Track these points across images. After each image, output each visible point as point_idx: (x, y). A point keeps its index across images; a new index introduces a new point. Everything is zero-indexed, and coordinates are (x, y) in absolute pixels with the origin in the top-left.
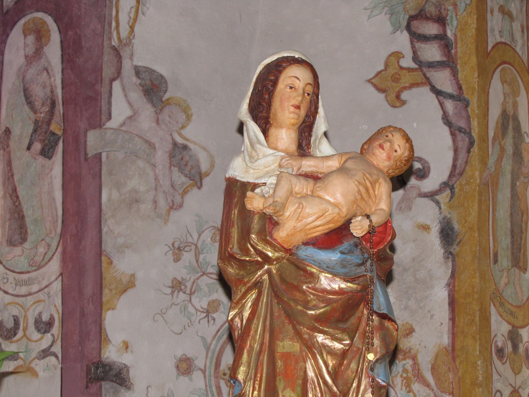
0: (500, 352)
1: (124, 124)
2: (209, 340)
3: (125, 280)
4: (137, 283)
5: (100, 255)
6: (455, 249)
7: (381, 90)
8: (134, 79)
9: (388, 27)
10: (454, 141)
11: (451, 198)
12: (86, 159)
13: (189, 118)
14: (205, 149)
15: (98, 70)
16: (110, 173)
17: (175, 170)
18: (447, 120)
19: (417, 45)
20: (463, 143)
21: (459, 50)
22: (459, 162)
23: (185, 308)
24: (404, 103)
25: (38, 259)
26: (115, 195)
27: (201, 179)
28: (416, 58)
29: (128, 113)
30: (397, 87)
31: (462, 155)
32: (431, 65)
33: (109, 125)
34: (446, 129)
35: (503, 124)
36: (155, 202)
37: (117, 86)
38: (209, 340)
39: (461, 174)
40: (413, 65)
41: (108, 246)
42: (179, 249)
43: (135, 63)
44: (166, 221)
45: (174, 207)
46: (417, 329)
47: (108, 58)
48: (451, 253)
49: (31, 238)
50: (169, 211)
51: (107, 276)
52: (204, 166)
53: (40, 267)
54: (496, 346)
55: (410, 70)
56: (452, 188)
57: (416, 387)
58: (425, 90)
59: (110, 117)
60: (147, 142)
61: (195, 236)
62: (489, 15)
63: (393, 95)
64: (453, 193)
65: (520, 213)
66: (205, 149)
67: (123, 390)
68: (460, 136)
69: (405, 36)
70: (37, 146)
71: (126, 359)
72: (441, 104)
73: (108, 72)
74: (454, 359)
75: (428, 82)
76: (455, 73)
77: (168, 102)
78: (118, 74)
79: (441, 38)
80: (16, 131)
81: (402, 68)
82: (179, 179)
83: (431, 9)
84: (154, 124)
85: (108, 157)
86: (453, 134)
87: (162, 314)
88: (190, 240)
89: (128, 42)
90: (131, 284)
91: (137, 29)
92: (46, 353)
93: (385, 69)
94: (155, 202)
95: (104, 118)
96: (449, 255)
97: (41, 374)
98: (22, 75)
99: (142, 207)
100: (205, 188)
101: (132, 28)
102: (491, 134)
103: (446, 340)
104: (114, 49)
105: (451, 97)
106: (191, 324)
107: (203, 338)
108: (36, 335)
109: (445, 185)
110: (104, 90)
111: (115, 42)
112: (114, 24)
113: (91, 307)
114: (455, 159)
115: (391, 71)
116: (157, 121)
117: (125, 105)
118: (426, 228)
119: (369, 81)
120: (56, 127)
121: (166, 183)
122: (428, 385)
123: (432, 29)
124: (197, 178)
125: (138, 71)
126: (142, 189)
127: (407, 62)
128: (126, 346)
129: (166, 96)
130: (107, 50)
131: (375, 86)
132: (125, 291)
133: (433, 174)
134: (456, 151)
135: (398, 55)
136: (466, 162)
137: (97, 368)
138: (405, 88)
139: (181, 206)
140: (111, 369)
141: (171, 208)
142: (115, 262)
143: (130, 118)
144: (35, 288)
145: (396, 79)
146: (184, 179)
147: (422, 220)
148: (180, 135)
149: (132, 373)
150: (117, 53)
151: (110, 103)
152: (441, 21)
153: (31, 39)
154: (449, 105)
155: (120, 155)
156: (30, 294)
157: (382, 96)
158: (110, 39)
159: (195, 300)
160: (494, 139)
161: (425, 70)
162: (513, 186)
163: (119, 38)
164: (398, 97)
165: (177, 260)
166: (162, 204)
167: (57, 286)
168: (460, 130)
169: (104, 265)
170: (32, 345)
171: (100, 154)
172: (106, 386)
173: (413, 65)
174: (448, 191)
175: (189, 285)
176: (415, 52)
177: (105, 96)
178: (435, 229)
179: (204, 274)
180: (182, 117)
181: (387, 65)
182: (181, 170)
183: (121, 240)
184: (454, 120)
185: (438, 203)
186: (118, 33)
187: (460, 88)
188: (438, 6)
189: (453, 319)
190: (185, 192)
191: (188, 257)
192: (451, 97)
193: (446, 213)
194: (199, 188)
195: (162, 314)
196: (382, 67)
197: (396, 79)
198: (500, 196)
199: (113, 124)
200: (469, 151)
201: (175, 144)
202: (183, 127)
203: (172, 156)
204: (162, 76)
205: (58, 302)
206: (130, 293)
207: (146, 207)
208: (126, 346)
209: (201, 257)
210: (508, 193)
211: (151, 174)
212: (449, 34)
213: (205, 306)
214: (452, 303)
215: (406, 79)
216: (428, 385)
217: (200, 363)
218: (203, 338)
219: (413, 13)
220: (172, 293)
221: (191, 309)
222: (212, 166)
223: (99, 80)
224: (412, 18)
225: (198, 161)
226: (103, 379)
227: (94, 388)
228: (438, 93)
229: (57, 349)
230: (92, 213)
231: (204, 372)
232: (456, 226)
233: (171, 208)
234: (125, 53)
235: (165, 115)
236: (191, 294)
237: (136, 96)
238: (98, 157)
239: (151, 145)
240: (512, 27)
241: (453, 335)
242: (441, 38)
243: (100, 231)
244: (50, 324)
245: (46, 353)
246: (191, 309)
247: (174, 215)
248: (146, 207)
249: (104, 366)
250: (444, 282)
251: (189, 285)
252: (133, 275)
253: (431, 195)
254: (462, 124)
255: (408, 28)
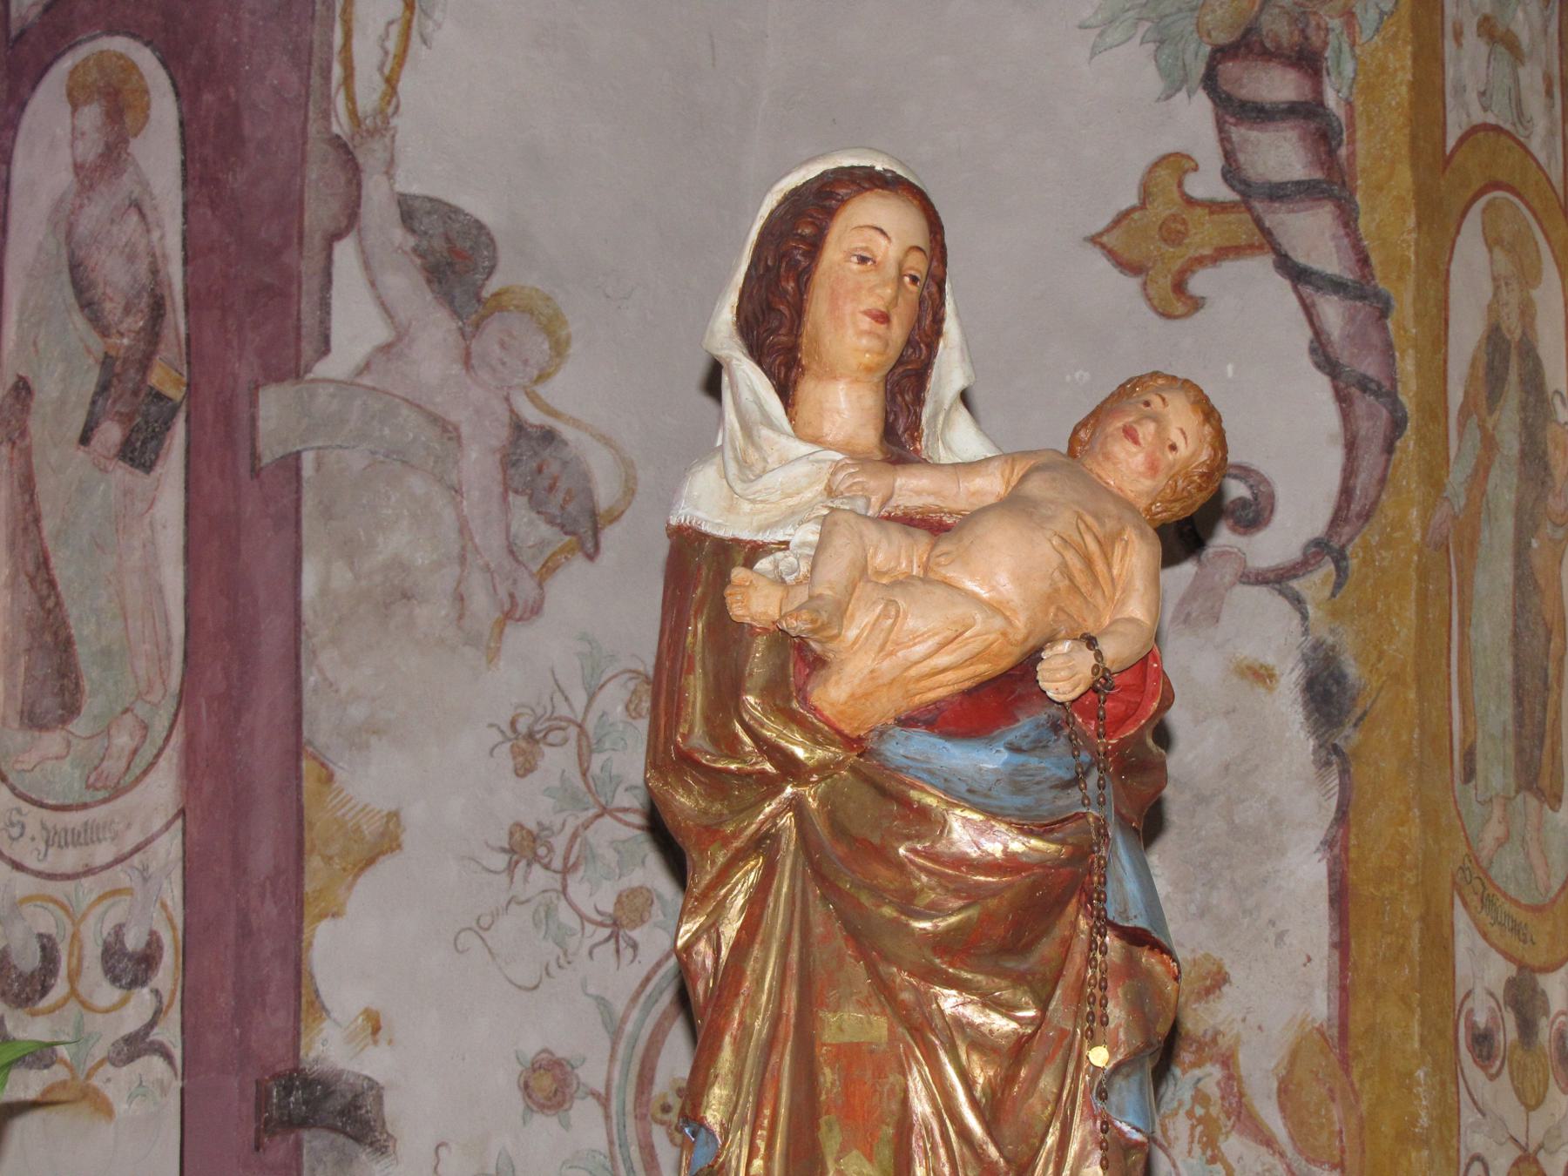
0: (1483, 1042)
1: (366, 367)
2: (619, 1007)
3: (370, 829)
4: (406, 839)
5: (298, 755)
6: (1349, 737)
7: (1130, 267)
8: (398, 234)
9: (1151, 80)
10: (1346, 416)
11: (1338, 586)
12: (255, 472)
13: (559, 348)
14: (607, 441)
15: (290, 207)
16: (327, 513)
17: (519, 502)
18: (1323, 356)
19: (1237, 133)
20: (1372, 425)
21: (1361, 148)
22: (1362, 481)
23: (550, 911)
24: (1196, 304)
25: (114, 766)
26: (342, 577)
27: (596, 532)
28: (1232, 173)
29: (380, 333)
30: (1176, 257)
31: (1370, 459)
32: (1279, 193)
33: (322, 369)
34: (1322, 382)
35: (1490, 368)
36: (460, 598)
37: (345, 254)
38: (619, 1007)
39: (1366, 516)
40: (1225, 194)
41: (320, 727)
42: (530, 736)
43: (400, 187)
44: (493, 655)
45: (515, 612)
46: (1236, 973)
47: (319, 171)
48: (1336, 749)
49: (92, 705)
50: (500, 626)
51: (318, 818)
52: (605, 493)
53: (117, 792)
54: (1472, 1026)
55: (1214, 207)
56: (1340, 558)
57: (1234, 1145)
58: (1261, 267)
59: (325, 348)
60: (437, 421)
61: (579, 698)
62: (1449, 44)
63: (1166, 282)
64: (1342, 572)
65: (1541, 631)
66: (607, 441)
67: (363, 1154)
68: (1363, 404)
69: (1202, 106)
70: (111, 434)
71: (373, 1064)
72: (1308, 310)
73: (319, 212)
74: (1345, 1063)
75: (1268, 242)
76: (1347, 218)
77: (498, 303)
78: (350, 218)
79: (1308, 112)
80: (47, 389)
81: (1190, 202)
82: (532, 529)
83: (1278, 28)
84: (457, 369)
85: (319, 465)
86: (1342, 398)
87: (480, 929)
88: (563, 710)
89: (381, 125)
90: (387, 841)
91: (405, 85)
92: (136, 1046)
93: (1143, 206)
94: (460, 598)
95: (308, 349)
96: (1332, 755)
97: (121, 1107)
98: (65, 224)
99: (422, 612)
100: (607, 556)
101: (391, 82)
102: (1456, 396)
103: (1321, 1007)
104: (338, 144)
105: (1337, 286)
106: (566, 959)
107: (602, 1002)
108: (107, 994)
109: (1319, 548)
110: (309, 267)
111: (340, 125)
112: (337, 71)
113: (271, 909)
114: (1349, 472)
115: (1160, 210)
116: (467, 360)
117: (372, 311)
118: (1261, 675)
119: (1094, 240)
120: (166, 377)
121: (491, 543)
122: (1269, 1142)
123: (1279, 86)
124: (585, 528)
125: (408, 211)
126: (421, 559)
127: (1207, 184)
128: (374, 1025)
129: (493, 285)
130: (317, 148)
131: (1111, 254)
132: (371, 861)
133: (1283, 516)
134: (1351, 446)
135: (1178, 163)
136: (1383, 481)
137: (288, 1090)
138: (1200, 261)
139: (536, 610)
140: (328, 1093)
141: (508, 616)
142: (341, 776)
143: (386, 349)
144: (103, 853)
145: (1173, 233)
146: (545, 530)
147: (1252, 650)
148: (534, 399)
149: (391, 1106)
150: (346, 156)
151: (325, 306)
152: (1308, 61)
153: (92, 115)
154: (1332, 311)
155: (356, 460)
156: (89, 871)
157: (1132, 284)
158: (326, 115)
159: (577, 889)
160: (1465, 412)
161: (1258, 206)
162: (1521, 552)
163: (353, 113)
164: (1179, 287)
165: (524, 769)
166: (481, 603)
167: (169, 847)
168: (1364, 384)
169: (309, 784)
170: (96, 1022)
171: (298, 455)
172: (315, 1142)
173: (1225, 194)
174: (1328, 567)
175: (560, 843)
176: (1229, 155)
177: (310, 285)
178: (1290, 678)
179: (604, 811)
180: (539, 347)
181: (1146, 193)
182: (537, 505)
183: (357, 712)
184: (1344, 356)
185: (1297, 601)
186: (351, 98)
187: (1364, 261)
188: (1299, 18)
189: (1342, 946)
190: (549, 569)
191: (557, 760)
192: (1337, 286)
193: (1322, 631)
194: (591, 557)
195: (480, 929)
196: (1132, 199)
197: (1173, 233)
198: (1481, 581)
199: (335, 366)
200: (1389, 449)
201: (519, 427)
202: (543, 377)
203: (508, 462)
204: (481, 227)
205: (173, 893)
206: (385, 867)
207: (432, 614)
208: (374, 1025)
209: (597, 762)
210: (1505, 570)
211: (449, 515)
212: (1332, 100)
213: (609, 908)
214: (1341, 896)
215: (1205, 234)
216: (1269, 1142)
217: (592, 1074)
218: (602, 1002)
219: (1223, 38)
220: (511, 868)
221: (565, 915)
222: (630, 491)
223: (295, 236)
224: (1221, 54)
225: (586, 477)
226: (304, 1123)
227: (278, 1149)
228: (1297, 275)
229: (170, 1033)
230: (272, 629)
231: (604, 1101)
232: (1353, 670)
233: (508, 616)
234: (371, 158)
235: (489, 342)
236: (566, 871)
237: (404, 284)
238: (292, 464)
239: (448, 431)
240: (1517, 80)
241: (1344, 993)
242: (1308, 112)
243: (297, 685)
244: (147, 960)
245: (136, 1046)
246: (565, 915)
247: (517, 636)
248: (432, 614)
249: (308, 1083)
250: (1317, 835)
251: (560, 843)
252: (394, 816)
253: (1278, 579)
254: (1370, 366)
255: (1210, 82)
